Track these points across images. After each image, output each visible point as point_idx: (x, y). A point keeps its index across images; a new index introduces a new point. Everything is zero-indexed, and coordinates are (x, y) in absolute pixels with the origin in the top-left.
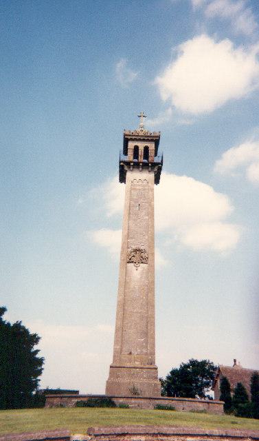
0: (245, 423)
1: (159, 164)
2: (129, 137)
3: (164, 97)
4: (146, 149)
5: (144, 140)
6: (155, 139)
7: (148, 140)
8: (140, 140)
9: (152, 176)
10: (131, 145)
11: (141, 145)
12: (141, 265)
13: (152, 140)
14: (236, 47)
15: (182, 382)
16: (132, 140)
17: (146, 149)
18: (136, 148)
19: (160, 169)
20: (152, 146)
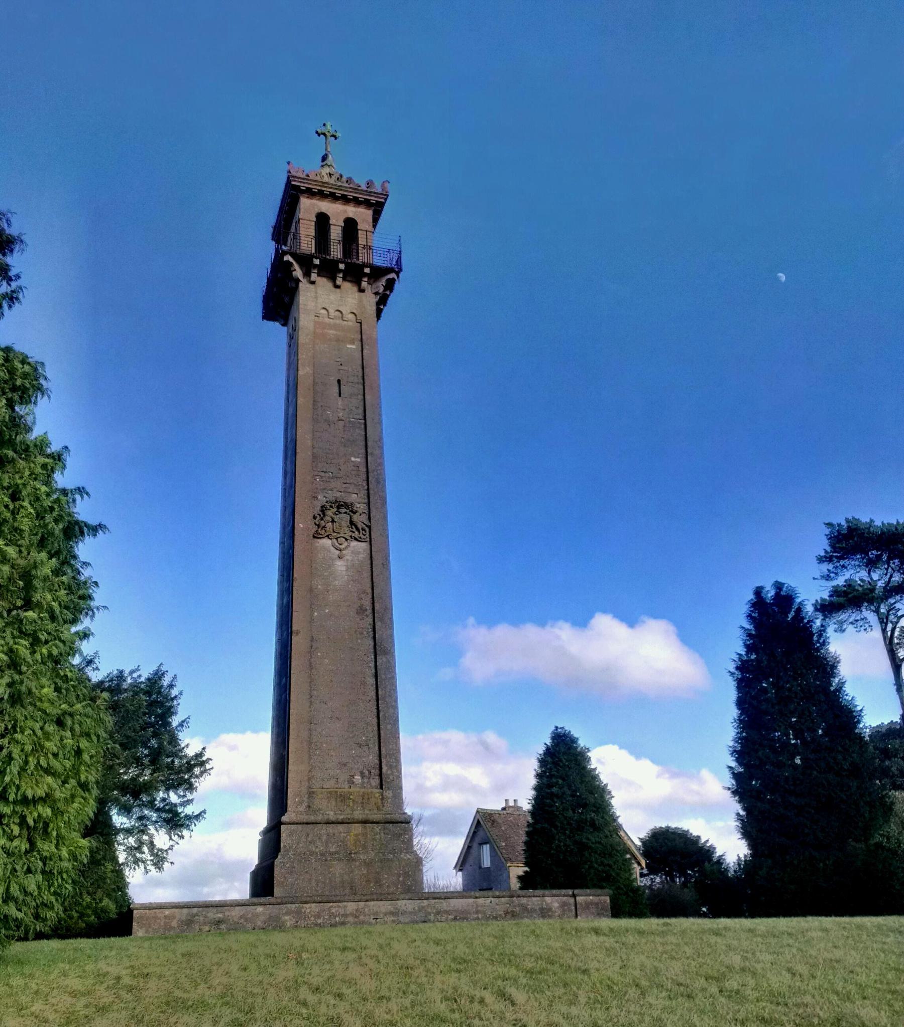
0: (381, 598)
1: (389, 270)
2: (303, 186)
3: (834, 615)
4: (350, 226)
5: (345, 200)
6: (373, 199)
7: (357, 202)
8: (333, 197)
9: (370, 300)
10: (308, 208)
11: (337, 212)
12: (354, 544)
13: (367, 204)
14: (172, 714)
15: (330, 878)
16: (310, 193)
17: (350, 226)
18: (322, 220)
19: (390, 285)
20: (363, 216)
